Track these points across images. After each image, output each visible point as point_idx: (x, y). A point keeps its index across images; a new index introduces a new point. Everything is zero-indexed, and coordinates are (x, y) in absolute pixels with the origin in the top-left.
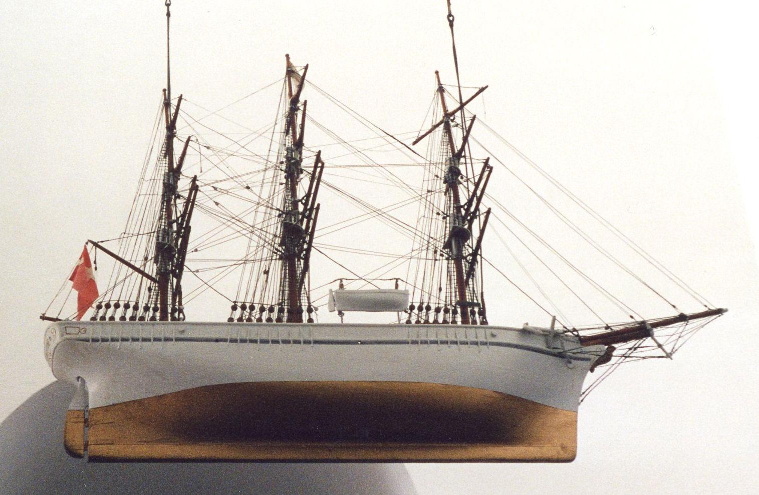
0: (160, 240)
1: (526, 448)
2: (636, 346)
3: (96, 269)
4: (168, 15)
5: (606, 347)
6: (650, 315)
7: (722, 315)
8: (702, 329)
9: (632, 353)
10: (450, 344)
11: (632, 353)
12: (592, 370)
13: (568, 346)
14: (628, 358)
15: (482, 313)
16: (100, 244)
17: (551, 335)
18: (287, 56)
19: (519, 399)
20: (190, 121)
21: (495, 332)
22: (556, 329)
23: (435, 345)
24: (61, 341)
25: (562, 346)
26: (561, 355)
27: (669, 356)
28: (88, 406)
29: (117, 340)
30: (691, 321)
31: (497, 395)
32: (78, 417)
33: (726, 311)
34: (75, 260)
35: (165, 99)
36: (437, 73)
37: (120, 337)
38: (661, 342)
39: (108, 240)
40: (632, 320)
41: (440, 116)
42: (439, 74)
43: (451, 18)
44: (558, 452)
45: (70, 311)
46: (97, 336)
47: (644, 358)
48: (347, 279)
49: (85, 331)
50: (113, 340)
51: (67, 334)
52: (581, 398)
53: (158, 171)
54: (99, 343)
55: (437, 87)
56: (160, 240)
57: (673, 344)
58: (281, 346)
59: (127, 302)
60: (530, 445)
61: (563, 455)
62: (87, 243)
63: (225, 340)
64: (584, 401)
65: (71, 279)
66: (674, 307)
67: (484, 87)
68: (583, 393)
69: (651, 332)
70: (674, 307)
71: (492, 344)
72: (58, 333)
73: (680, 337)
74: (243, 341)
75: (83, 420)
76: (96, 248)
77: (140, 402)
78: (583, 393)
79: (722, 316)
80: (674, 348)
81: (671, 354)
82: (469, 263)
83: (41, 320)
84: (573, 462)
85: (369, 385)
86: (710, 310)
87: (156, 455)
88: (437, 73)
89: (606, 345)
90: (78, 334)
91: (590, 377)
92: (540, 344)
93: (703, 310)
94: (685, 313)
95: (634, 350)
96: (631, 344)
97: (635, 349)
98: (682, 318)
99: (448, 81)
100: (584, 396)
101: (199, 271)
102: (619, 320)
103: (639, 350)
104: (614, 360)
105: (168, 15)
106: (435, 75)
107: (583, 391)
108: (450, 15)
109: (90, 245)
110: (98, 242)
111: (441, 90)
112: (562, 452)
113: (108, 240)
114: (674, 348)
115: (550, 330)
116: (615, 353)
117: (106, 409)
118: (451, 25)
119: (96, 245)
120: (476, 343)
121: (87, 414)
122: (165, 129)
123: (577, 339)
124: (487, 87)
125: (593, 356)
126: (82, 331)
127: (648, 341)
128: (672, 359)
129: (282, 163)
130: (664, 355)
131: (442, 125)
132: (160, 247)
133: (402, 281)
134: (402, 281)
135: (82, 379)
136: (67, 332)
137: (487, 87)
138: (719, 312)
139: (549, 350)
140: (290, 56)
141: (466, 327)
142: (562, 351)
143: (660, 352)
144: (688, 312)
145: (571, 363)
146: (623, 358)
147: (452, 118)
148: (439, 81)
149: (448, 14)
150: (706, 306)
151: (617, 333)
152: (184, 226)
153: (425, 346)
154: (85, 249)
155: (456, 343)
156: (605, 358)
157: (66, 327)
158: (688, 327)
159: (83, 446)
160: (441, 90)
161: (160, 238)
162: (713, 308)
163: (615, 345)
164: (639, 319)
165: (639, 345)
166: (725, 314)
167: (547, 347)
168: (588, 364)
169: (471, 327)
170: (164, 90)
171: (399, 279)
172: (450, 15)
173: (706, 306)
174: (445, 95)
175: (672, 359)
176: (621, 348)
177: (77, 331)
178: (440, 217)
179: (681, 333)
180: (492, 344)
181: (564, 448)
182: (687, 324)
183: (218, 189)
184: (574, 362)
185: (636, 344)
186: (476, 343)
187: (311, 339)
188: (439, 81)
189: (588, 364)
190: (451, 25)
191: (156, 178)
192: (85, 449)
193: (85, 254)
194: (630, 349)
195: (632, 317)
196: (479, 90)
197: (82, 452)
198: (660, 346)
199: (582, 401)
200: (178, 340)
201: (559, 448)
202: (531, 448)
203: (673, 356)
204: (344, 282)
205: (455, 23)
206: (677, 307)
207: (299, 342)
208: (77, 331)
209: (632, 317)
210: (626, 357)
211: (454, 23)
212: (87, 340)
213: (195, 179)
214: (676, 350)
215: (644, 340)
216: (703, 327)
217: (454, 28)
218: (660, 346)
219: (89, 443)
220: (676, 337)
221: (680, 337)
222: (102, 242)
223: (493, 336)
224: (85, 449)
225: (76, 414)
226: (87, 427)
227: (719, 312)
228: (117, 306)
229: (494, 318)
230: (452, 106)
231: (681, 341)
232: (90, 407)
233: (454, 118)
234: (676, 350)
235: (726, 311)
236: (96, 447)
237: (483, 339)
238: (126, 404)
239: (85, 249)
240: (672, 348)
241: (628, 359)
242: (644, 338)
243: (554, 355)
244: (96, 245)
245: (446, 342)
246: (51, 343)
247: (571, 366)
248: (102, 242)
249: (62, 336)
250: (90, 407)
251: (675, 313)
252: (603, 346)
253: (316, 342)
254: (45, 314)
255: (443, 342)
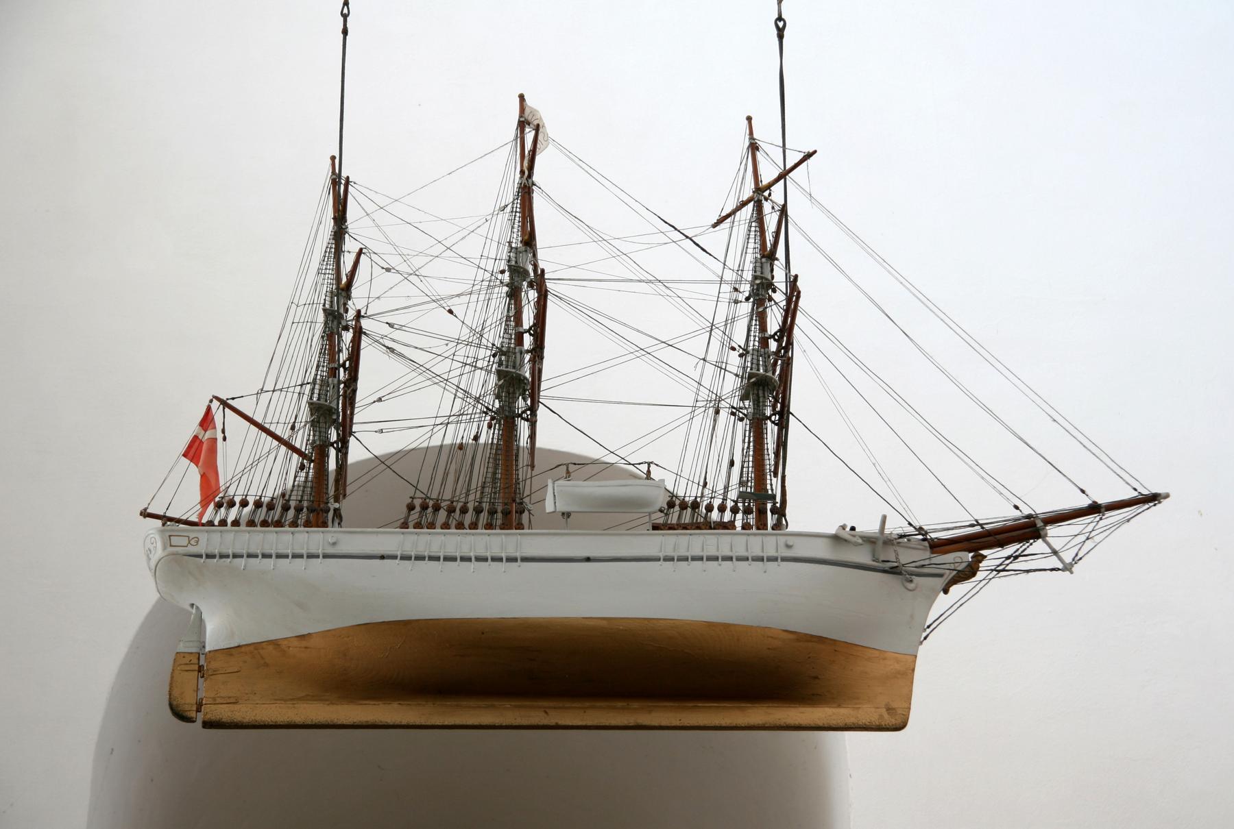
0: (315, 399)
1: (834, 710)
2: (1017, 554)
3: (225, 439)
4: (345, 32)
5: (971, 554)
6: (1042, 505)
7: (1160, 503)
8: (1127, 525)
9: (1011, 563)
10: (722, 560)
11: (1011, 563)
12: (946, 591)
13: (906, 557)
14: (1001, 573)
15: (780, 512)
16: (230, 402)
17: (878, 542)
18: (522, 97)
19: (821, 640)
20: (370, 207)
21: (791, 541)
22: (887, 531)
23: (699, 563)
24: (163, 555)
25: (897, 558)
26: (894, 571)
27: (1068, 568)
28: (204, 647)
29: (242, 556)
30: (1108, 514)
31: (791, 636)
32: (190, 663)
33: (1167, 496)
34: (189, 428)
35: (333, 172)
36: (749, 119)
37: (245, 552)
38: (1057, 548)
39: (242, 397)
40: (1017, 514)
41: (748, 192)
42: (753, 122)
43: (781, 24)
44: (881, 716)
45: (187, 502)
46: (213, 551)
47: (1028, 571)
48: (575, 464)
49: (197, 542)
50: (235, 556)
51: (171, 546)
52: (924, 635)
53: (315, 290)
54: (215, 560)
55: (747, 143)
56: (315, 399)
57: (1075, 550)
58: (473, 565)
59: (258, 498)
60: (839, 706)
61: (888, 720)
62: (211, 401)
63: (394, 557)
64: (928, 639)
65: (185, 455)
66: (1083, 491)
67: (811, 151)
68: (929, 627)
69: (1042, 533)
70: (1083, 491)
71: (784, 559)
72: (159, 545)
73: (1088, 539)
74: (420, 558)
75: (196, 667)
76: (224, 408)
77: (275, 643)
78: (929, 627)
79: (1158, 506)
80: (1077, 555)
81: (1071, 565)
82: (776, 424)
83: (142, 517)
84: (907, 727)
85: (604, 623)
86: (1142, 495)
87: (298, 719)
88: (749, 119)
89: (970, 552)
90: (187, 546)
91: (942, 602)
92: (863, 557)
93: (1130, 494)
94: (1100, 502)
95: (1014, 560)
96: (1010, 550)
97: (1016, 558)
98: (1094, 509)
99: (767, 133)
100: (928, 631)
101: (384, 431)
102: (997, 512)
103: (1021, 559)
104: (980, 575)
105: (345, 32)
106: (746, 122)
107: (928, 623)
108: (780, 18)
109: (216, 404)
110: (227, 399)
111: (754, 147)
112: (886, 716)
113: (242, 397)
114: (1077, 555)
115: (878, 535)
116: (983, 564)
117: (228, 652)
118: (781, 36)
119: (224, 404)
120: (761, 559)
121: (202, 657)
122: (332, 221)
123: (926, 543)
124: (815, 152)
125: (948, 572)
126: (192, 542)
127: (1038, 546)
128: (1072, 573)
129: (503, 272)
130: (1060, 566)
131: (751, 204)
132: (314, 408)
133: (657, 465)
134: (657, 465)
135: (197, 608)
136: (173, 544)
137: (815, 152)
138: (1154, 498)
139: (874, 563)
140: (525, 97)
141: (748, 535)
142: (896, 564)
143: (1054, 562)
144: (1102, 500)
145: (911, 581)
146: (995, 573)
147: (766, 194)
148: (751, 133)
149: (777, 16)
150: (1135, 490)
151: (989, 533)
152: (342, 386)
153: (684, 563)
154: (209, 409)
155: (730, 559)
156: (968, 573)
157: (170, 536)
158: (1102, 523)
159: (195, 706)
160: (754, 147)
161: (316, 396)
162: (1145, 492)
163: (984, 552)
164: (1027, 511)
165: (1022, 552)
166: (1165, 502)
167: (874, 561)
168: (940, 582)
169: (755, 535)
170: (333, 158)
171: (652, 463)
172: (780, 18)
173: (1135, 490)
174: (759, 155)
175: (1072, 573)
176: (993, 556)
177: (184, 541)
178: (736, 354)
179: (1091, 532)
180: (784, 559)
181: (889, 709)
182: (1101, 519)
183: (395, 326)
184: (916, 579)
185: (1018, 550)
186: (761, 559)
187: (518, 555)
188: (751, 133)
189: (940, 582)
190: (781, 36)
191: (315, 302)
192: (198, 710)
193: (207, 421)
194: (1008, 558)
195: (1016, 507)
196: (804, 156)
197: (193, 714)
198: (1055, 553)
199: (925, 638)
200: (326, 556)
201: (884, 711)
202: (842, 711)
203: (1075, 568)
204: (572, 468)
205: (786, 33)
206: (1088, 491)
207: (500, 560)
208: (184, 541)
209: (1016, 507)
210: (999, 571)
211: (785, 33)
212: (200, 556)
213: (359, 312)
214: (1081, 559)
215: (1031, 544)
216: (1128, 520)
217: (785, 40)
218: (1055, 553)
219: (204, 702)
220: (1083, 538)
221: (1088, 539)
222: (233, 399)
223: (788, 547)
224: (198, 710)
225: (186, 660)
226: (201, 677)
227: (1154, 498)
228: (244, 503)
229: (796, 520)
230: (768, 173)
231: (1089, 544)
232: (208, 649)
233: (770, 195)
234: (1081, 559)
235: (1167, 496)
236: (213, 707)
237: (772, 553)
238: (257, 646)
239: (209, 409)
240: (1074, 555)
241: (1002, 574)
242: (1031, 541)
243: (884, 571)
244: (224, 404)
245: (716, 559)
246: (151, 556)
247: (911, 586)
248: (233, 399)
249: (165, 548)
250: (208, 649)
251: (1084, 502)
252: (967, 553)
253: (525, 559)
254: (147, 508)
255: (710, 559)
